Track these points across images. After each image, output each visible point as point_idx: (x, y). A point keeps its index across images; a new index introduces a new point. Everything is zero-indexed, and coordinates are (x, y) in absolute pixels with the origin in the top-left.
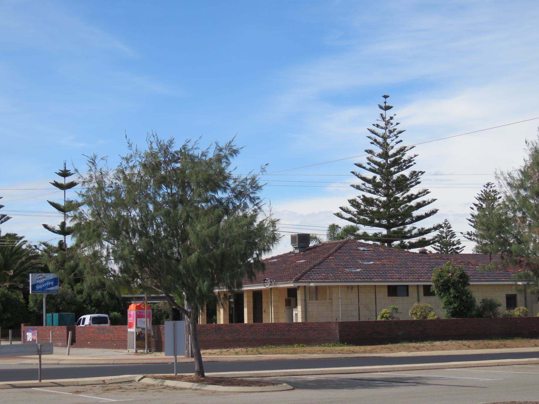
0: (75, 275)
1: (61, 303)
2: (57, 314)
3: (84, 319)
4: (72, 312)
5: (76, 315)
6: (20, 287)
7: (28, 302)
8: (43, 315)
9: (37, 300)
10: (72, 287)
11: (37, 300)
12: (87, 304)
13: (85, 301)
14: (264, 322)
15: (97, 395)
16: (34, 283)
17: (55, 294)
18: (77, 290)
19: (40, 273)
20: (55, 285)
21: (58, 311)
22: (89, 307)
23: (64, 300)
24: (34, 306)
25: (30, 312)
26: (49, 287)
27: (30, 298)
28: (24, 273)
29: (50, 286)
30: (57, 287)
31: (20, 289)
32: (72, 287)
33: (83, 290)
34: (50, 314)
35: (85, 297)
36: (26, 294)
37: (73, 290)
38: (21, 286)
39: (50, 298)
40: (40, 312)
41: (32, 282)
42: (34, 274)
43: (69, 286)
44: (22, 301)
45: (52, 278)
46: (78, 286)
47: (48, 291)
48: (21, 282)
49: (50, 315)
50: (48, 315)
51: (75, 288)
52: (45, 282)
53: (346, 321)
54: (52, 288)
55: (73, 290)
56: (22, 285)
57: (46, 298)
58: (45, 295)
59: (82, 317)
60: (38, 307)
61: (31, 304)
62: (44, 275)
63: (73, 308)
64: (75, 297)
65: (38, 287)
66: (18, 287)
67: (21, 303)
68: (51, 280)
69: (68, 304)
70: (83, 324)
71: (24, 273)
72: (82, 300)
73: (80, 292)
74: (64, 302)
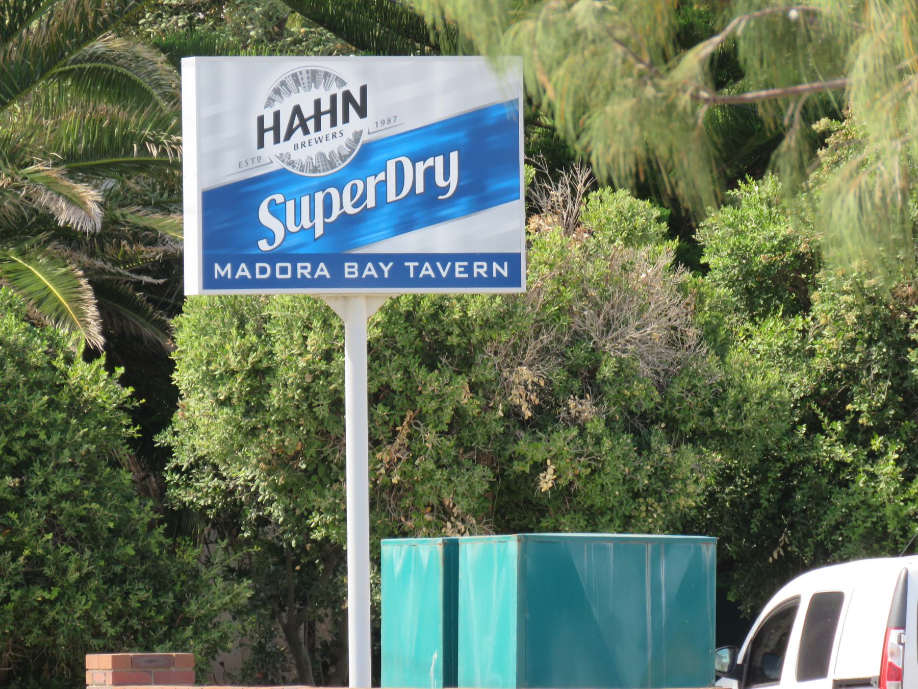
0: (725, 68)
1: (546, 416)
2: (511, 543)
3: (827, 609)
4: (686, 525)
5: (725, 565)
6: (65, 215)
7: (155, 396)
8: (334, 555)
9: (260, 375)
10: (681, 224)
11: (260, 375)
12: (855, 435)
13: (830, 398)
14: (888, 682)
15: (127, 652)
16: (229, 173)
17: (480, 300)
18: (740, 254)
19: (298, 47)
20: (478, 194)
21: (512, 507)
22: (887, 468)
23: (587, 378)
24: (231, 452)
25: (180, 521)
26: (405, 225)
27: (190, 345)
28: (109, 43)
29: (428, 206)
30: (498, 227)
31: (68, 237)
32: (681, 224)
33: (809, 262)
34: (429, 549)
35: (831, 341)
36: (139, 314)
37: (690, 257)
38: (83, 205)
39: (420, 345)
40: (298, 520)
41: (207, 159)
42: (228, 65)
43: (648, 212)
44: (100, 385)
45: (442, 109)
46: (748, 221)
47: (399, 269)
48: (80, 165)
49: (414, 558)
50: (391, 548)
51: (715, 230)
52: (365, 157)
53: (515, 678)
54: (440, 238)
55: (690, 257)
56: (90, 195)
57: (374, 352)
58: (360, 315)
59: (804, 587)
60: (279, 461)
61: (200, 424)
62: (350, 70)
63: (697, 470)
64: (718, 341)
65: (275, 224)
66: (46, 220)
67: (79, 408)
68: (426, 142)
69: (637, 424)
70: (815, 661)
71: (109, 43)
72: (799, 383)
73: (783, 284)
74: (584, 408)
